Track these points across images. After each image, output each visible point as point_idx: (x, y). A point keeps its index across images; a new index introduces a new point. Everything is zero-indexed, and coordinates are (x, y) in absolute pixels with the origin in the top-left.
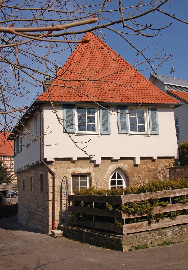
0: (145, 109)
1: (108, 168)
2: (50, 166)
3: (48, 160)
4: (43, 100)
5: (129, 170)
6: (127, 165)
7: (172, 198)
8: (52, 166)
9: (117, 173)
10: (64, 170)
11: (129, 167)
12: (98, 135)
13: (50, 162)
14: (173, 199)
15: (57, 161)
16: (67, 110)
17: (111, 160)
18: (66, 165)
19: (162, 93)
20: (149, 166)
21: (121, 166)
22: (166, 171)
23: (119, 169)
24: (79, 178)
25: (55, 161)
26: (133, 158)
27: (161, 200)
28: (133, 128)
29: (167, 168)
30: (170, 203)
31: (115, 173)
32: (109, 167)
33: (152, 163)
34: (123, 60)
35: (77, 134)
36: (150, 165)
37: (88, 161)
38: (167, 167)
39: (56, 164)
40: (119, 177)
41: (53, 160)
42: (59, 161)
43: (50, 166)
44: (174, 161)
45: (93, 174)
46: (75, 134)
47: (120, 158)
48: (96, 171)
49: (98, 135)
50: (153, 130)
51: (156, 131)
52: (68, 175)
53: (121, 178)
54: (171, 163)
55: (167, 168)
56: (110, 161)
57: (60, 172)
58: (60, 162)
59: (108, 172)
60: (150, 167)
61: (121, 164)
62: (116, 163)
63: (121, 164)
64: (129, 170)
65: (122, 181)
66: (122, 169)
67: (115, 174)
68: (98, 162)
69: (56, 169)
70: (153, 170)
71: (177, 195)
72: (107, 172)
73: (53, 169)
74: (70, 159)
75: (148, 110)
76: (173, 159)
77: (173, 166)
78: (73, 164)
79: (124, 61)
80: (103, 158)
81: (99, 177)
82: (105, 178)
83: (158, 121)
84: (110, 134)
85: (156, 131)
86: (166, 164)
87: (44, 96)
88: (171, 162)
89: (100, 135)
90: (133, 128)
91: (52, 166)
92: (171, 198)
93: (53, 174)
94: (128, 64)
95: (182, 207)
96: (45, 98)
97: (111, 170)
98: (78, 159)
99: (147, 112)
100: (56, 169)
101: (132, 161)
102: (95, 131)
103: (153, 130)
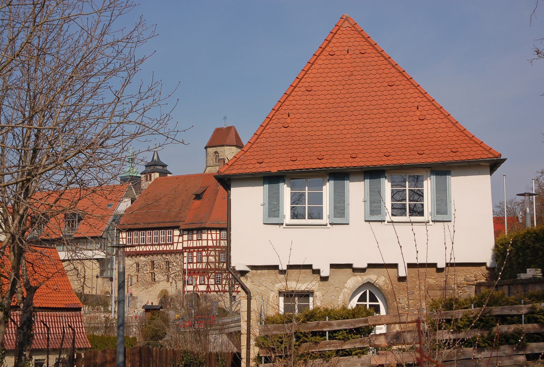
0: (426, 172)
1: (346, 282)
2: (243, 279)
3: (238, 268)
4: (227, 173)
5: (388, 287)
6: (383, 277)
7: (329, 332)
8: (247, 279)
9: (370, 292)
10: (266, 285)
11: (388, 282)
12: (326, 225)
13: (243, 273)
14: (333, 334)
15: (254, 271)
16: (271, 185)
17: (351, 269)
18: (270, 277)
19: (469, 138)
20: (431, 280)
21: (372, 280)
22: (467, 290)
23: (369, 284)
24: (297, 299)
25: (250, 270)
26: (395, 266)
27: (314, 334)
28: (398, 210)
29: (470, 285)
30: (325, 339)
31: (365, 293)
32: (349, 281)
33: (437, 275)
34: (401, 73)
35: (287, 225)
36: (433, 279)
37: (308, 270)
38: (469, 283)
39: (253, 275)
40: (373, 298)
41: (248, 269)
42: (258, 271)
43: (243, 279)
44: (487, 272)
45: (317, 293)
46: (284, 225)
47: (366, 266)
48: (324, 288)
49: (326, 225)
50: (438, 213)
51: (445, 213)
52: (273, 295)
53: (378, 302)
54: (481, 276)
55: (470, 285)
56: (350, 270)
57: (260, 288)
58: (259, 271)
59: (345, 290)
60: (431, 281)
61: (372, 276)
62: (362, 274)
63: (372, 276)
64: (388, 287)
65: (379, 306)
66: (375, 284)
67: (365, 293)
68: (325, 272)
69: (254, 284)
70: (438, 289)
71: (336, 328)
72: (343, 291)
73: (248, 284)
74: (276, 267)
75: (429, 175)
76: (483, 268)
77: (483, 281)
78: (282, 276)
79: (402, 74)
80: (333, 266)
81: (328, 297)
82: (339, 299)
83: (450, 196)
84: (348, 224)
85: (445, 213)
86: (468, 276)
87: (232, 165)
88: (479, 273)
89: (329, 226)
90: (398, 210)
91: (247, 279)
92: (327, 333)
93: (247, 292)
94: (410, 82)
95: (341, 346)
96: (232, 168)
97: (351, 287)
98: (290, 267)
99: (428, 179)
100: (254, 284)
101: (394, 270)
102: (322, 219)
103: (438, 213)
